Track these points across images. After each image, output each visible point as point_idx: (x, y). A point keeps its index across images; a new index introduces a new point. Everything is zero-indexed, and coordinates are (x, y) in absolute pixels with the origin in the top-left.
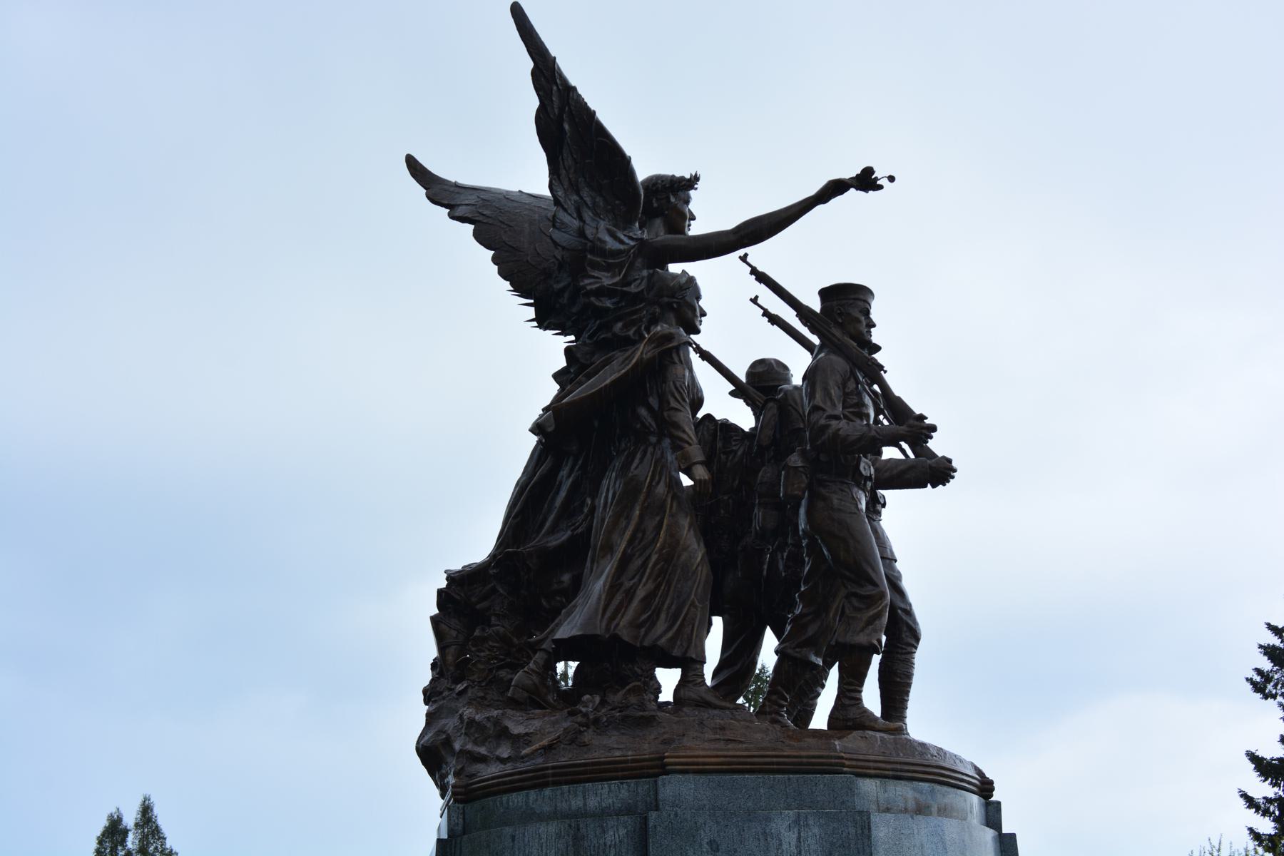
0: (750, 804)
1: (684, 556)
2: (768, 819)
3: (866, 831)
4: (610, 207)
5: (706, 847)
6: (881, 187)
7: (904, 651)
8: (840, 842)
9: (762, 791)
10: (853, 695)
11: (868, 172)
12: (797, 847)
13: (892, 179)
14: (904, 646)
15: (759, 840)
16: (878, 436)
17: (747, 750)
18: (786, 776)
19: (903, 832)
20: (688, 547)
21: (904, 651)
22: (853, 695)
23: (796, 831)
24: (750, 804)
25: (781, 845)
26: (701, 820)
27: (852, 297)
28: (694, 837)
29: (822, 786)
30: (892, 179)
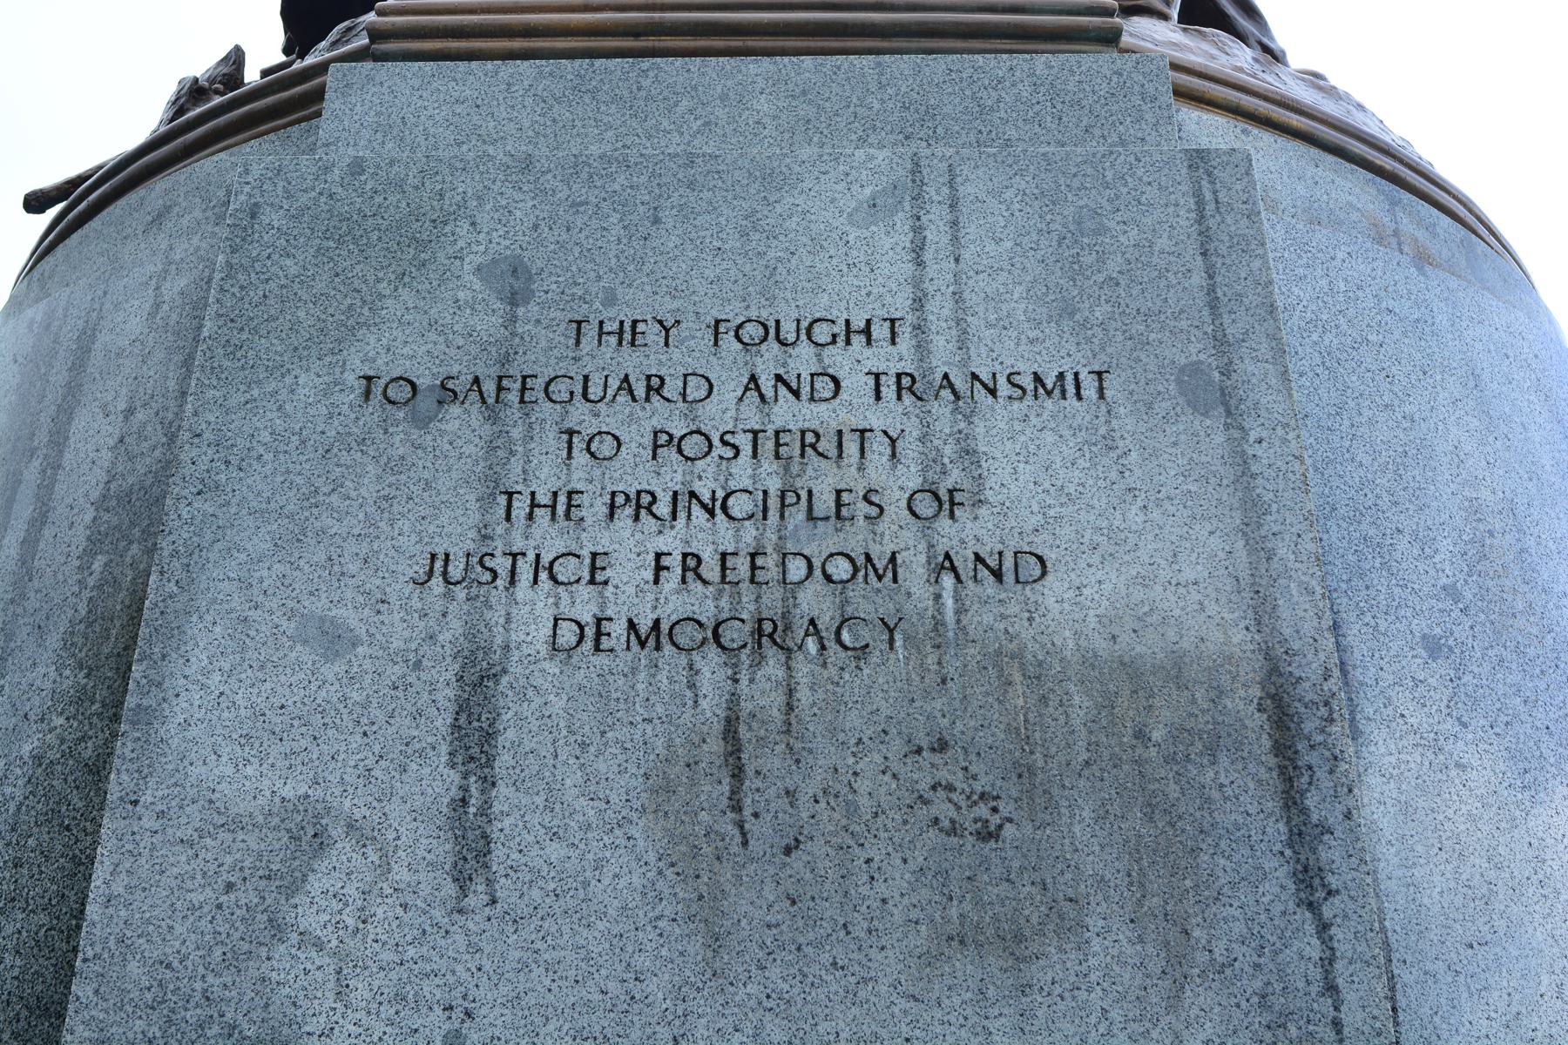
23: (902, 221)
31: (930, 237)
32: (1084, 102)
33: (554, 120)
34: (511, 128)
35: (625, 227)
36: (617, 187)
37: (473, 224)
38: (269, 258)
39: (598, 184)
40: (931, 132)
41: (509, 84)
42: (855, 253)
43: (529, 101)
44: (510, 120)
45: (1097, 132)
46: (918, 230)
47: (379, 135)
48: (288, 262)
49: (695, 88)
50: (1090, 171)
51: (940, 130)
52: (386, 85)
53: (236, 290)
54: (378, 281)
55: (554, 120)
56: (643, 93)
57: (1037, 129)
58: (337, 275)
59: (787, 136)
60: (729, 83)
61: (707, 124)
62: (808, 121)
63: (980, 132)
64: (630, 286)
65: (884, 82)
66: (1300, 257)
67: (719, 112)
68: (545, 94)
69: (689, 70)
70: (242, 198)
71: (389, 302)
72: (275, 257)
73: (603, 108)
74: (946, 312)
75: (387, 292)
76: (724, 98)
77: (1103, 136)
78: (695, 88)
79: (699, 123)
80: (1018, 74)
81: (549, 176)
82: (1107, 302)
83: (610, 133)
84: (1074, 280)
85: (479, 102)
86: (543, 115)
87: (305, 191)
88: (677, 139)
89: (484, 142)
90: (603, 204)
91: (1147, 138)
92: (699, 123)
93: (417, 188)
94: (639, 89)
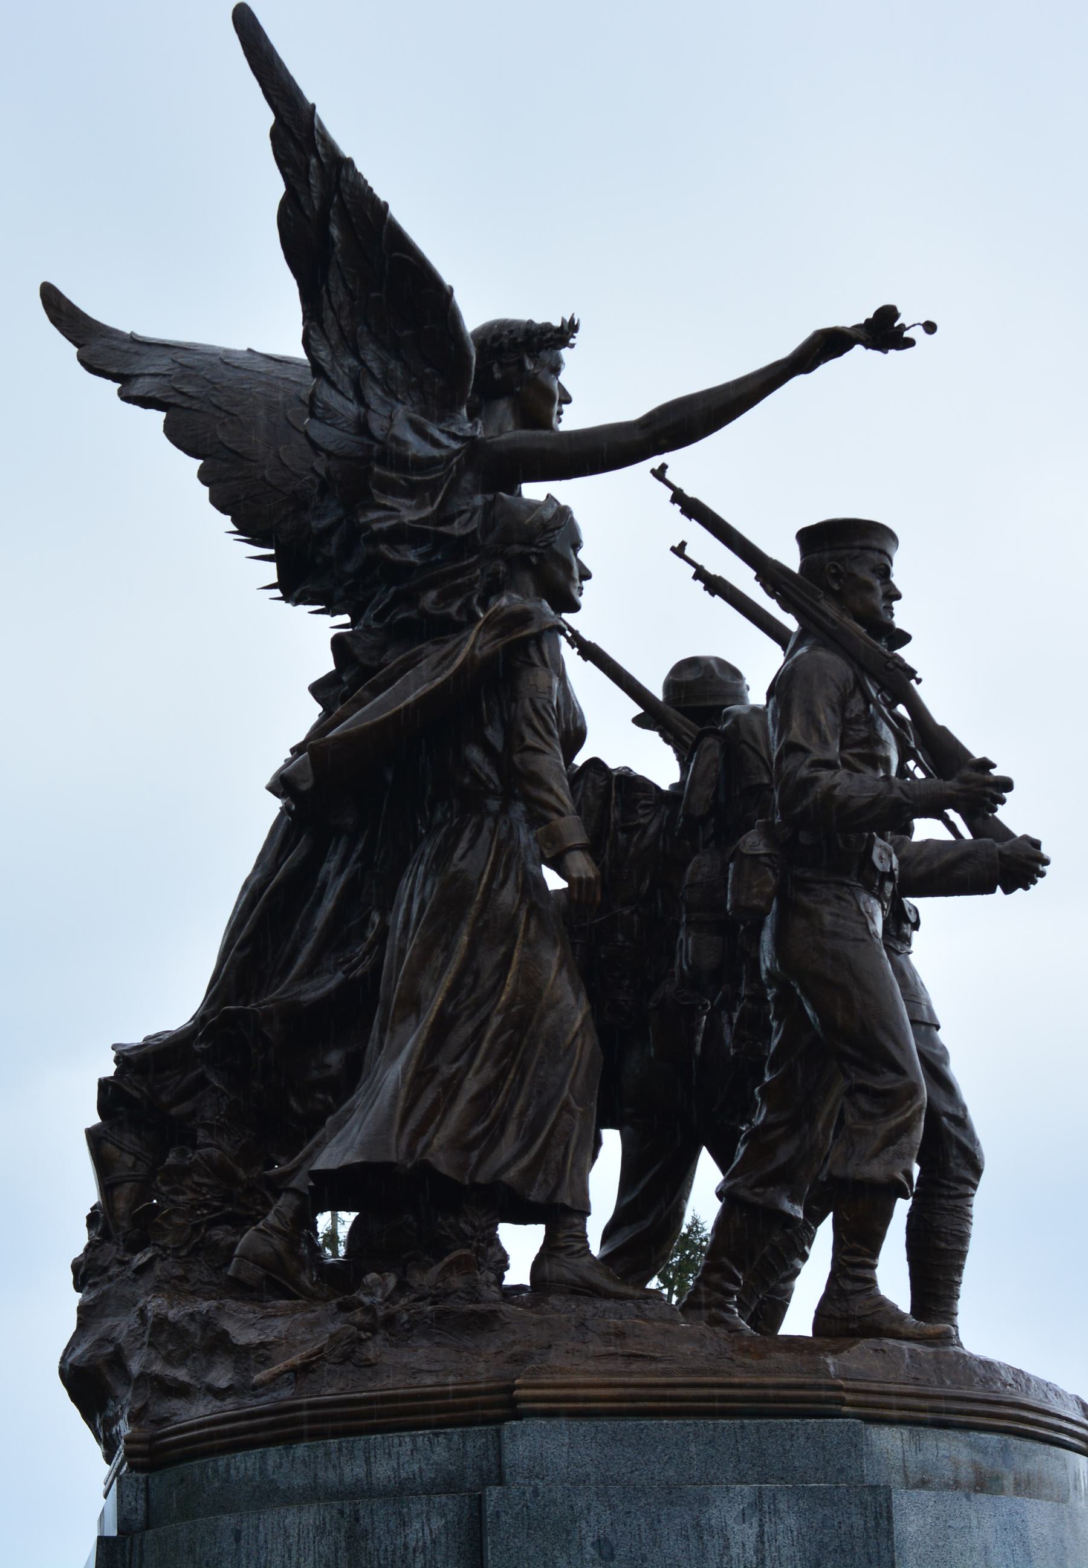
0: (671, 1473)
1: (551, 1019)
2: (704, 1501)
3: (884, 1523)
4: (414, 379)
5: (590, 1552)
6: (910, 343)
7: (952, 1193)
8: (837, 1542)
9: (693, 1448)
10: (860, 1272)
11: (887, 315)
12: (757, 1551)
13: (930, 327)
14: (952, 1184)
15: (687, 1538)
16: (905, 799)
17: (665, 1373)
18: (738, 1422)
19: (951, 1523)
20: (558, 1003)
21: (952, 1193)
22: (860, 1272)
23: (755, 1521)
24: (671, 1473)
25: (727, 1547)
26: (581, 1503)
27: (858, 543)
28: (568, 1533)
29: (802, 1440)
30: (930, 327)
31: (766, 1530)
32: (827, 1447)
33: (606, 1456)
34: (588, 1459)
35: (647, 1524)
36: (642, 1504)
37: (587, 1522)
38: (508, 1538)
39: (634, 1502)
40: (763, 1463)
41: (585, 1436)
42: (737, 1537)
43: (594, 1445)
44: (587, 1455)
45: (832, 1463)
46: (761, 1526)
47: (532, 1462)
48: (517, 1540)
49: (664, 1439)
50: (828, 1497)
51: (767, 1462)
52: (531, 1435)
53: (498, 1554)
54: (554, 1549)
55: (606, 1456)
56: (642, 1442)
57: (807, 1461)
58: (537, 1547)
59: (704, 1464)
60: (678, 1436)
61: (670, 1458)
62: (713, 1457)
63: (784, 1463)
64: (652, 1553)
65: (744, 1436)
66: (912, 1510)
67: (676, 1452)
68: (600, 1441)
69: (661, 1430)
70: (491, 1508)
71: (560, 1560)
72: (511, 1538)
73: (626, 1449)
74: (772, 1366)
75: (558, 1555)
76: (676, 1444)
77: (834, 1466)
78: (664, 1439)
79: (667, 1457)
80: (800, 1432)
81: (614, 1498)
82: (833, 1560)
83: (629, 1463)
84: (820, 1550)
85: (572, 1445)
86: (600, 1453)
87: (516, 1505)
88: (658, 1466)
89: (577, 1467)
90: (638, 1513)
91: (853, 1466)
92: (667, 1457)
93: (561, 1503)
94: (640, 1439)
